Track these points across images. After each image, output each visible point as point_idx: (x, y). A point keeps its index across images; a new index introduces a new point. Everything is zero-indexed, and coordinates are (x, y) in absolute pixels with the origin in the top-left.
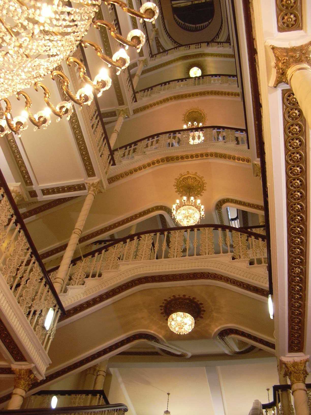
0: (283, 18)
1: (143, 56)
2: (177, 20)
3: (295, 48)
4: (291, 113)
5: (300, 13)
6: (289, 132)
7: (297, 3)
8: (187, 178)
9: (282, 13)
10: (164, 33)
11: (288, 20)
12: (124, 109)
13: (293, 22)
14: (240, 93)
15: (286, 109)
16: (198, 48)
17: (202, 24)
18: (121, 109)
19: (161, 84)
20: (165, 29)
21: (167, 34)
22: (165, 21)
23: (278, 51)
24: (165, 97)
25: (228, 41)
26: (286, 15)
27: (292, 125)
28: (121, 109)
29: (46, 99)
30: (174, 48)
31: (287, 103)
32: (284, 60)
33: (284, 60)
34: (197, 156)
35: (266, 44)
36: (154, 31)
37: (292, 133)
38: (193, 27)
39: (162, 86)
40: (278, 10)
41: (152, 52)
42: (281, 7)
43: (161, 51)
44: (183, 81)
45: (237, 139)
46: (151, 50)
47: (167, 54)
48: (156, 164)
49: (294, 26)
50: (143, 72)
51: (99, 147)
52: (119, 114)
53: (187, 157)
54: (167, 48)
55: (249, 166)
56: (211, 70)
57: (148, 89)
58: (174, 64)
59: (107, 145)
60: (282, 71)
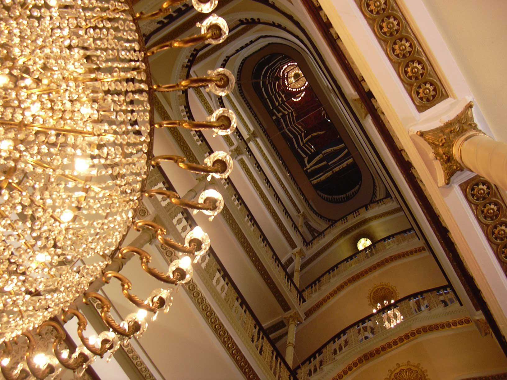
0: (418, 93)
1: (296, 247)
2: (324, 197)
3: (450, 122)
4: (485, 211)
5: (436, 77)
6: (496, 238)
7: (427, 67)
8: (400, 373)
9: (414, 87)
10: (313, 215)
11: (425, 92)
12: (292, 314)
13: (432, 93)
14: (425, 246)
15: (476, 210)
16: (357, 216)
17: (353, 191)
18: (289, 316)
19: (328, 271)
20: (314, 212)
21: (316, 215)
22: (310, 202)
23: (429, 135)
24: (338, 284)
25: (388, 195)
26: (420, 87)
27: (495, 227)
28: (289, 316)
29: (125, 291)
30: (330, 227)
31: (474, 200)
32: (442, 140)
33: (442, 140)
34: (401, 340)
35: (411, 133)
36: (300, 216)
37: (499, 238)
38: (344, 197)
39: (330, 273)
40: (406, 86)
41: (306, 240)
42: (409, 80)
43: (316, 235)
44: (353, 259)
45: (443, 301)
46: (303, 238)
47: (324, 236)
48: (354, 369)
49: (437, 96)
50: (303, 267)
51: (273, 369)
52: (289, 322)
53: (389, 346)
54: (321, 229)
55: (472, 327)
56: (381, 234)
57: (314, 283)
58: (336, 245)
59: (282, 364)
60: (446, 156)
